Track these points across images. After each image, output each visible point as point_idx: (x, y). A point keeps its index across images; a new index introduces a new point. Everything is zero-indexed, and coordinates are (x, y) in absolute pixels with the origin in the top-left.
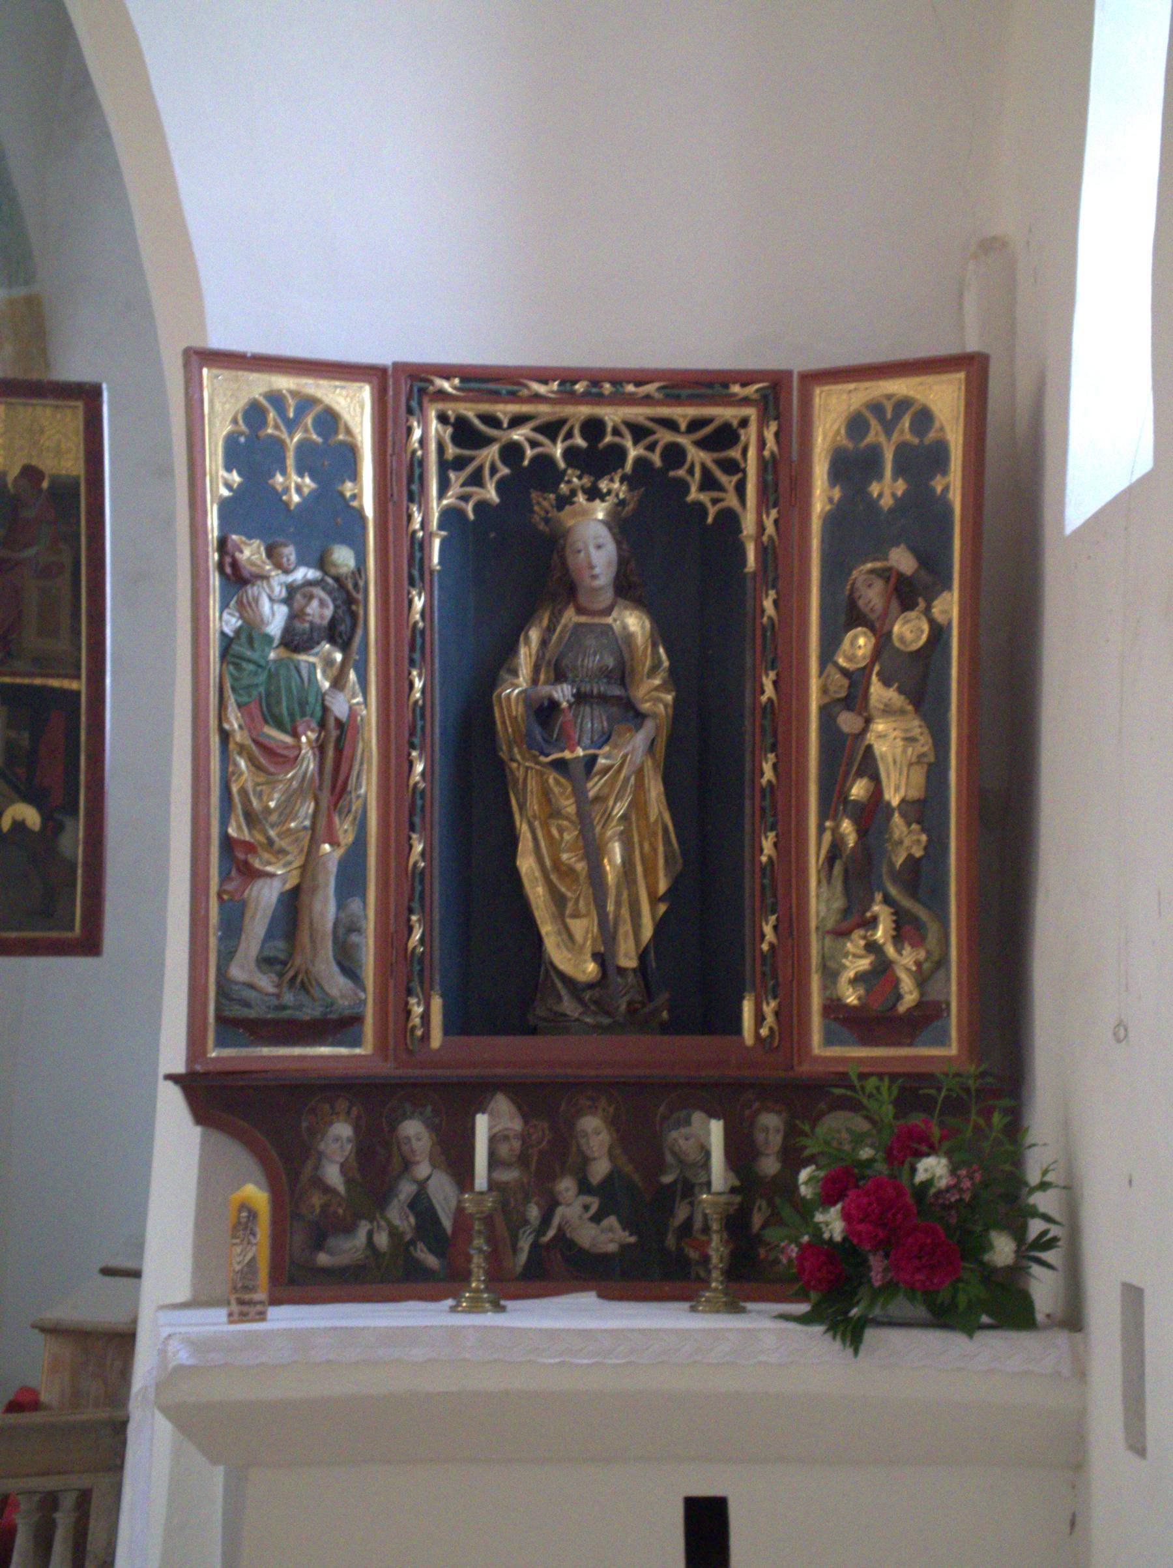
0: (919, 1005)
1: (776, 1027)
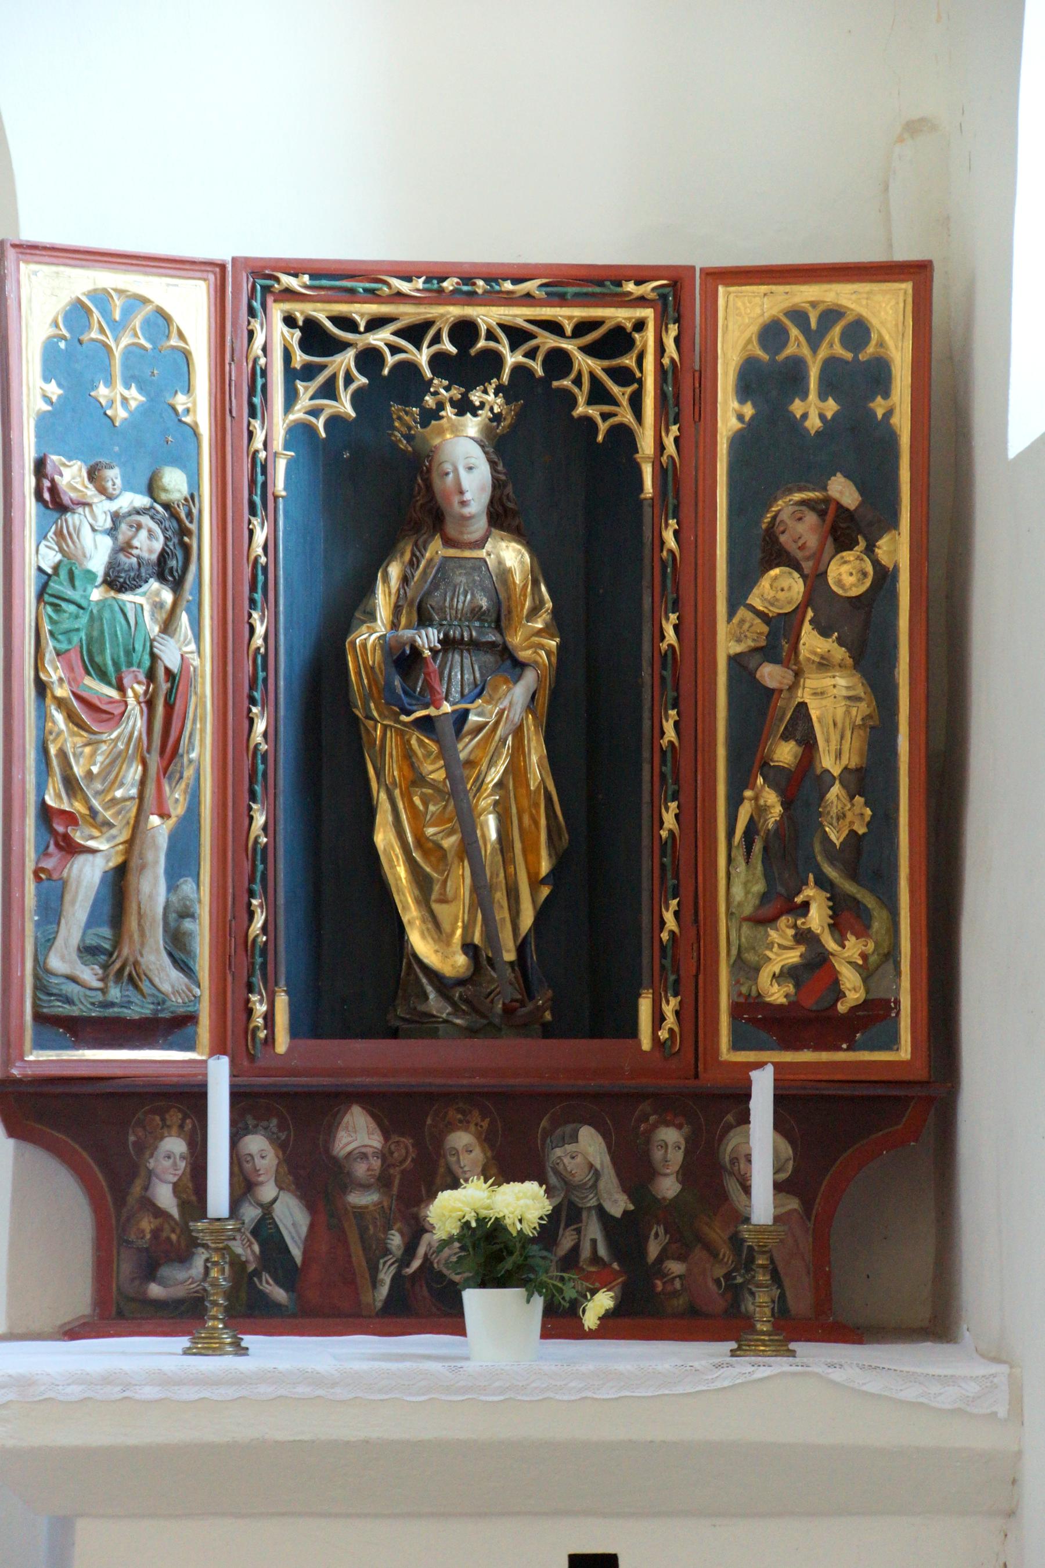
0: (865, 1004)
1: (676, 1029)
